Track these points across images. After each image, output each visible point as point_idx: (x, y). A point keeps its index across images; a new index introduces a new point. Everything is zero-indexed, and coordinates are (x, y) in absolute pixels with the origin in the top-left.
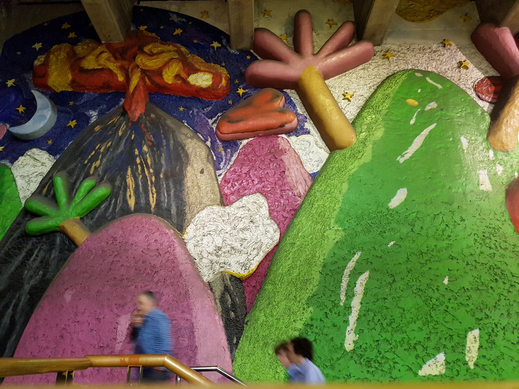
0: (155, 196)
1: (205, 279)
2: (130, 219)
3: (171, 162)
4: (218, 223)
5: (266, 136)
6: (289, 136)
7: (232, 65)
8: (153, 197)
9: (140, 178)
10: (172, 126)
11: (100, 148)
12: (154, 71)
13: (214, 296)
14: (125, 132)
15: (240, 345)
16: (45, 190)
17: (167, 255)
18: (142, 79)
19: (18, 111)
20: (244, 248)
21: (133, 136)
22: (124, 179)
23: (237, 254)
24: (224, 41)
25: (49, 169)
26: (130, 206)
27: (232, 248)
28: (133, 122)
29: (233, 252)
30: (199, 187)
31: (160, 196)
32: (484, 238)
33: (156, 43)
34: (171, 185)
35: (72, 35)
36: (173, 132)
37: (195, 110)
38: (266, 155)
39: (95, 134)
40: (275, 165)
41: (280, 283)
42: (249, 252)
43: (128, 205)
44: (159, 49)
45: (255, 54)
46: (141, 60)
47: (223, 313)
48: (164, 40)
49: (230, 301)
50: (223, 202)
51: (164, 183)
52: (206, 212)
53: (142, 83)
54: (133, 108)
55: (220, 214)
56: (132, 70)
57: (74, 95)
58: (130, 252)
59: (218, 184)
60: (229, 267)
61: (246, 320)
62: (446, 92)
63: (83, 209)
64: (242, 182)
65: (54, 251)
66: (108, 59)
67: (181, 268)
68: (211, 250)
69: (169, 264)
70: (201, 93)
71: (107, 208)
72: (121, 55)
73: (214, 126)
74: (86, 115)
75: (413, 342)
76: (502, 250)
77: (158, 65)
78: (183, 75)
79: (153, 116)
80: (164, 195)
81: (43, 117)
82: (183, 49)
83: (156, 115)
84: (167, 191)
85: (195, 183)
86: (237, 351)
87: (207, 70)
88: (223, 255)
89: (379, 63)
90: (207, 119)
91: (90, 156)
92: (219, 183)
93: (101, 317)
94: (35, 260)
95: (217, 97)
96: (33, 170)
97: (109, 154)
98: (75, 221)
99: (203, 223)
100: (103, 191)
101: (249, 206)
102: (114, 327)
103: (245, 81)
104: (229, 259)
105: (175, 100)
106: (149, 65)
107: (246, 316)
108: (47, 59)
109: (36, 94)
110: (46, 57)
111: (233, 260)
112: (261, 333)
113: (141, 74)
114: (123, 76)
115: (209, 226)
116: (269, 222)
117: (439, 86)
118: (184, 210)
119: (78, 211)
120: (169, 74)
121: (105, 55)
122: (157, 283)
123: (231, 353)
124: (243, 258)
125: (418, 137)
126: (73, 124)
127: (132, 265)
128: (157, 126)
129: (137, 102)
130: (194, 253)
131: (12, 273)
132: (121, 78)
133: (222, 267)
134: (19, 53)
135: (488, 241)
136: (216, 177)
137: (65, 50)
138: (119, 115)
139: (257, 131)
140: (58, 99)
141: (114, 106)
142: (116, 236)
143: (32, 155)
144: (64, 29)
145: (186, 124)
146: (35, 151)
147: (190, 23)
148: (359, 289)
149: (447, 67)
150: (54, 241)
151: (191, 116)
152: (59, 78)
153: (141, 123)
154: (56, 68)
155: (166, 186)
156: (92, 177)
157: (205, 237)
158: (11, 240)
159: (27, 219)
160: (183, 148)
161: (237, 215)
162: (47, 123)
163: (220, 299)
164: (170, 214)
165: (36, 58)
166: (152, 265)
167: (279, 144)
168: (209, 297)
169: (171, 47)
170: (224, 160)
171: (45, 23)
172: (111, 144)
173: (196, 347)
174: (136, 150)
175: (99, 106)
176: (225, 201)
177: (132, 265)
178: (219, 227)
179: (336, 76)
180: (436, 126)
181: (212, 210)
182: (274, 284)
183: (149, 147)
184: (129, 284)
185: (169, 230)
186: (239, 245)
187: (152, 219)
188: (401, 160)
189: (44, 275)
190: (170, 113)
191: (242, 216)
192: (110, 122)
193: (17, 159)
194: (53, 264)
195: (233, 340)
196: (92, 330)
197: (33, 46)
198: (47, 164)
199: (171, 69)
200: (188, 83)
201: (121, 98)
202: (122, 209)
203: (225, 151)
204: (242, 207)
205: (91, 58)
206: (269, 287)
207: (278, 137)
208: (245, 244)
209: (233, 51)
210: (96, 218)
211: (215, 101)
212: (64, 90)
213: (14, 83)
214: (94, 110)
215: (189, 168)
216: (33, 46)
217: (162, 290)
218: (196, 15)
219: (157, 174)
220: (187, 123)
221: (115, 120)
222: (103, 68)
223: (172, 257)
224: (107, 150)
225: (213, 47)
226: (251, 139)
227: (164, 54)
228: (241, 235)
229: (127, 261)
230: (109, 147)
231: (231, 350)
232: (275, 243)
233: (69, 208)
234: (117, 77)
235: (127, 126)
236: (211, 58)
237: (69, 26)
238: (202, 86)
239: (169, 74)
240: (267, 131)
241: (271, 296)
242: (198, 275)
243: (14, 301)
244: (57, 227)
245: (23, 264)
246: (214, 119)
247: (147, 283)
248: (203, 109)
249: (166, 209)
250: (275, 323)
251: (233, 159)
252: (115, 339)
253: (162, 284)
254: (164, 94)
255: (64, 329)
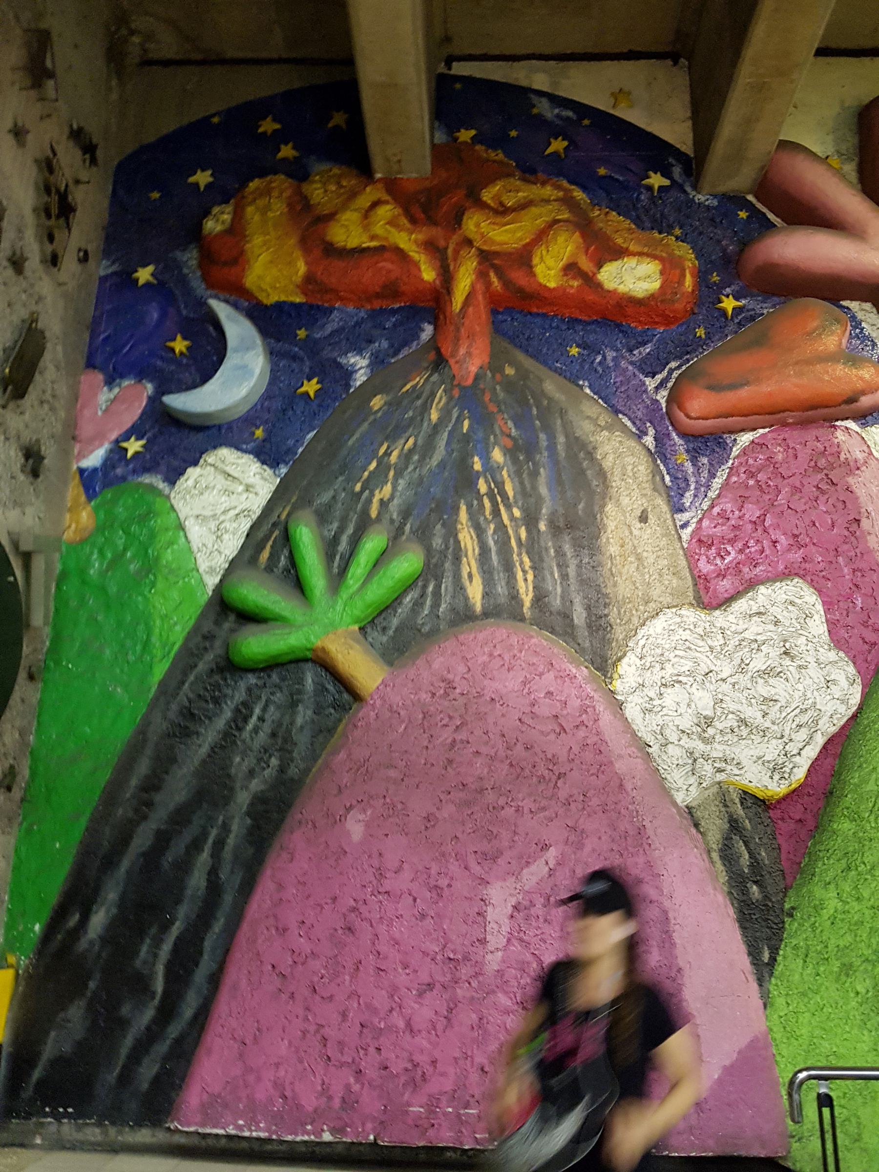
0: (530, 577)
1: (680, 798)
2: (481, 636)
3: (563, 492)
4: (698, 655)
5: (804, 424)
6: (864, 425)
7: (701, 233)
8: (526, 580)
9: (490, 532)
10: (558, 396)
11: (387, 454)
12: (510, 254)
14: (446, 413)
15: (779, 969)
16: (265, 554)
17: (582, 733)
18: (482, 274)
19: (173, 350)
20: (773, 723)
21: (466, 423)
22: (452, 533)
23: (757, 739)
24: (677, 171)
26: (472, 601)
27: (743, 722)
28: (465, 388)
29: (745, 732)
30: (639, 558)
31: (543, 579)
33: (512, 180)
34: (568, 548)
35: (287, 151)
36: (562, 413)
37: (610, 354)
38: (805, 474)
39: (372, 418)
41: (872, 818)
42: (787, 733)
43: (466, 598)
44: (520, 194)
45: (759, 206)
46: (478, 225)
47: (731, 886)
48: (529, 172)
49: (747, 857)
52: (665, 624)
53: (480, 287)
55: (700, 630)
56: (456, 252)
57: (308, 313)
60: (737, 772)
61: (787, 906)
63: (369, 606)
65: (300, 708)
66: (392, 223)
67: (620, 766)
68: (686, 723)
69: (588, 756)
71: (418, 604)
72: (424, 212)
73: (662, 397)
74: (339, 366)
77: (521, 239)
78: (585, 264)
79: (509, 371)
80: (552, 574)
81: (244, 369)
82: (579, 194)
83: (517, 370)
84: (559, 566)
85: (629, 547)
87: (646, 250)
88: (718, 738)
90: (641, 376)
91: (366, 474)
92: (686, 546)
93: (443, 882)
94: (256, 730)
95: (668, 321)
96: (225, 502)
99: (659, 651)
100: (408, 564)
101: (776, 611)
104: (737, 751)
105: (557, 327)
106: (498, 239)
107: (785, 896)
109: (222, 310)
111: (748, 752)
112: (833, 941)
113: (479, 263)
114: (434, 269)
116: (832, 655)
118: (606, 616)
119: (357, 612)
120: (550, 262)
121: (385, 211)
123: (760, 986)
124: (772, 750)
126: (311, 387)
127: (502, 753)
128: (521, 394)
129: (471, 336)
130: (643, 728)
131: (204, 762)
132: (428, 274)
133: (720, 770)
134: (156, 195)
136: (677, 531)
138: (427, 369)
139: (784, 411)
140: (273, 322)
141: (406, 343)
143: (219, 464)
144: (265, 133)
145: (588, 391)
146: (225, 453)
147: (586, 122)
151: (600, 369)
152: (274, 269)
153: (483, 391)
154: (265, 243)
155: (556, 551)
156: (377, 527)
157: (669, 690)
158: (192, 678)
159: (226, 626)
160: (590, 455)
161: (746, 635)
162: (255, 385)
163: (721, 850)
164: (572, 626)
165: (207, 213)
166: (549, 756)
168: (696, 847)
169: (548, 191)
170: (692, 487)
171: (213, 115)
172: (415, 444)
174: (476, 459)
175: (370, 341)
177: (502, 753)
178: (702, 665)
181: (678, 620)
182: (856, 818)
183: (506, 451)
184: (502, 801)
185: (577, 667)
186: (759, 715)
189: (282, 770)
190: (545, 363)
191: (759, 638)
192: (408, 387)
193: (182, 473)
195: (761, 953)
196: (423, 916)
197: (192, 179)
198: (258, 489)
199: (554, 249)
200: (599, 285)
203: (694, 460)
204: (759, 614)
205: (350, 217)
206: (844, 826)
207: (834, 427)
208: (774, 712)
209: (700, 198)
210: (397, 632)
212: (283, 298)
213: (152, 275)
214: (360, 352)
215: (609, 508)
216: (192, 179)
217: (581, 821)
218: (602, 103)
219: (530, 520)
220: (590, 387)
221: (418, 380)
223: (595, 739)
224: (406, 457)
225: (650, 188)
226: (761, 431)
228: (763, 690)
229: (487, 743)
231: (759, 979)
232: (850, 713)
233: (335, 603)
234: (419, 270)
235: (451, 398)
236: (654, 218)
237: (277, 126)
239: (550, 262)
240: (810, 413)
241: (851, 849)
242: (664, 791)
243: (214, 833)
244: (308, 650)
245: (229, 737)
246: (659, 377)
247: (544, 802)
250: (867, 917)
251: (717, 482)
252: (483, 941)
253: (580, 807)
254: (531, 314)
255: (354, 909)
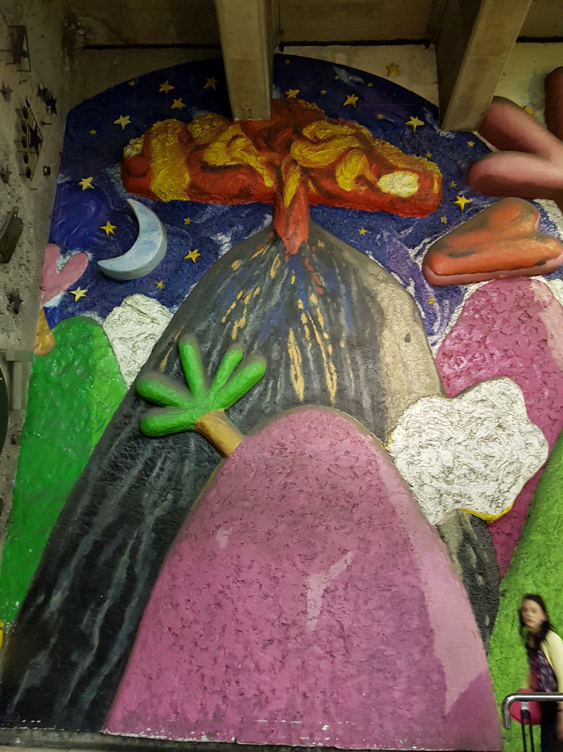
0: (335, 377)
1: (432, 520)
2: (303, 415)
5: (510, 278)
6: (549, 279)
10: (353, 261)
11: (243, 298)
13: (449, 549)
14: (280, 272)
15: (496, 630)
16: (164, 363)
17: (368, 478)
18: (303, 183)
20: (492, 471)
21: (293, 278)
23: (481, 481)
24: (428, 116)
25: (164, 329)
27: (472, 470)
28: (292, 255)
29: (473, 477)
30: (405, 365)
35: (178, 104)
36: (355, 271)
37: (386, 234)
39: (233, 275)
40: (528, 328)
41: (556, 532)
42: (500, 478)
43: (294, 391)
45: (482, 138)
46: (300, 151)
49: (475, 557)
50: (444, 390)
51: (347, 356)
52: (422, 408)
54: (291, 232)
55: (444, 411)
56: (287, 168)
58: (309, 469)
59: (433, 358)
64: (474, 357)
65: (187, 462)
67: (393, 499)
68: (436, 471)
69: (372, 492)
70: (398, 206)
71: (263, 394)
72: (266, 142)
73: (419, 261)
74: (212, 242)
77: (328, 160)
78: (370, 176)
79: (321, 245)
80: (349, 375)
82: (365, 131)
85: (398, 358)
86: (492, 637)
87: (408, 167)
88: (456, 481)
90: (406, 248)
91: (229, 311)
93: (279, 574)
94: (158, 476)
95: (423, 212)
96: (138, 329)
97: (258, 307)
98: (218, 414)
99: (418, 425)
100: (256, 369)
102: (301, 592)
103: (468, 183)
104: (468, 489)
105: (352, 217)
106: (314, 160)
108: (147, 145)
109: (136, 206)
110: (144, 143)
113: (302, 175)
115: (428, 431)
116: (530, 427)
118: (384, 402)
119: (223, 400)
120: (347, 175)
121: (241, 142)
122: (359, 523)
123: (484, 641)
124: (491, 489)
126: (193, 255)
127: (317, 491)
129: (296, 222)
130: (407, 475)
132: (269, 183)
133: (457, 502)
134: (93, 132)
137: (174, 130)
139: (494, 271)
140: (168, 212)
141: (254, 227)
142: (283, 441)
145: (371, 257)
147: (370, 85)
150: (187, 445)
151: (379, 244)
152: (170, 179)
153: (304, 257)
154: (164, 162)
155: (352, 361)
159: (139, 409)
161: (474, 414)
163: (458, 553)
165: (127, 143)
167: (533, 292)
169: (345, 129)
170: (439, 319)
171: (131, 81)
172: (260, 292)
173: (432, 631)
174: (300, 301)
175: (231, 226)
176: (450, 390)
178: (446, 433)
181: (430, 405)
183: (319, 296)
184: (317, 522)
185: (365, 435)
186: (482, 466)
187: (335, 416)
189: (175, 502)
190: (344, 240)
192: (256, 255)
194: (188, 482)
195: (484, 619)
197: (116, 122)
199: (350, 166)
200: (379, 190)
201: (265, 212)
202: (285, 398)
203: (440, 302)
204: (482, 401)
205: (218, 146)
206: (537, 537)
207: (530, 280)
208: (492, 464)
209: (443, 133)
210: (249, 413)
211: (419, 218)
212: (175, 198)
214: (225, 233)
215: (386, 333)
216: (116, 122)
219: (335, 340)
220: (373, 255)
221: (262, 251)
222: (240, 165)
224: (255, 300)
225: (411, 127)
226: (483, 283)
227: (336, 141)
228: (485, 450)
230: (257, 296)
232: (541, 464)
233: (209, 394)
235: (283, 262)
236: (413, 146)
237: (172, 88)
238: (401, 195)
242: (421, 515)
244: (192, 424)
245: (141, 481)
246: (417, 249)
247: (344, 523)
248: (399, 231)
249: (353, 401)
251: (455, 316)
254: (334, 207)
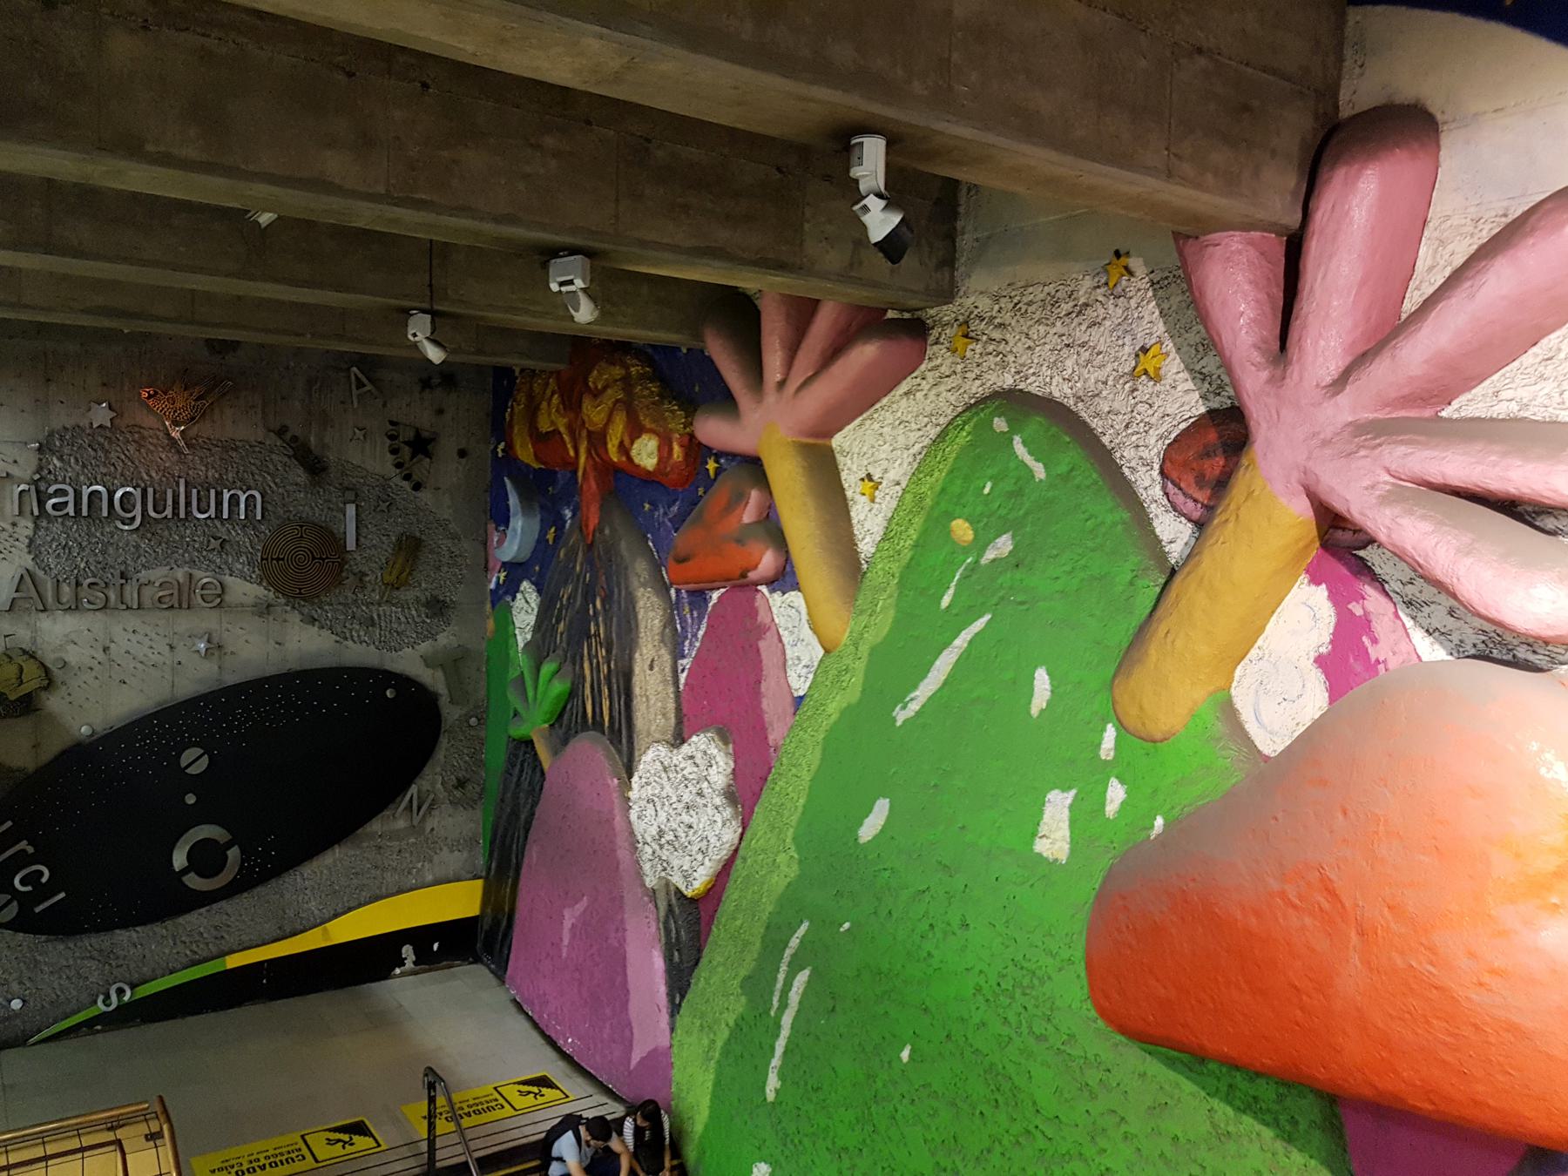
32: (997, 989)
62: (1050, 494)
75: (840, 1143)
76: (1032, 1040)
89: (943, 369)
117: (1039, 471)
125: (945, 653)
132: (572, 453)
135: (1004, 1000)
148: (794, 997)
149: (1101, 374)
179: (853, 419)
180: (989, 621)
188: (901, 716)
242: (639, 875)
